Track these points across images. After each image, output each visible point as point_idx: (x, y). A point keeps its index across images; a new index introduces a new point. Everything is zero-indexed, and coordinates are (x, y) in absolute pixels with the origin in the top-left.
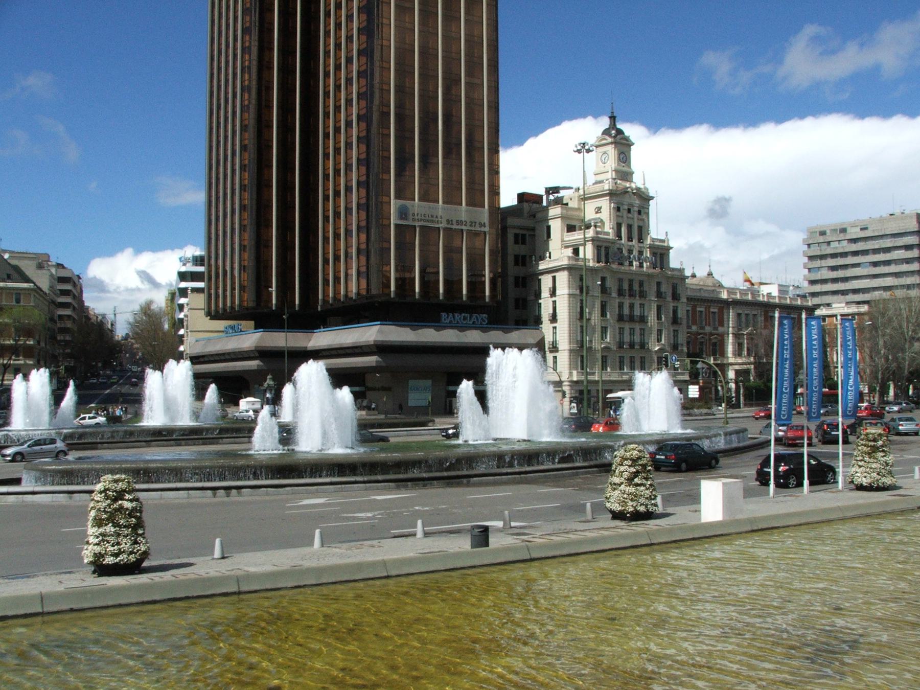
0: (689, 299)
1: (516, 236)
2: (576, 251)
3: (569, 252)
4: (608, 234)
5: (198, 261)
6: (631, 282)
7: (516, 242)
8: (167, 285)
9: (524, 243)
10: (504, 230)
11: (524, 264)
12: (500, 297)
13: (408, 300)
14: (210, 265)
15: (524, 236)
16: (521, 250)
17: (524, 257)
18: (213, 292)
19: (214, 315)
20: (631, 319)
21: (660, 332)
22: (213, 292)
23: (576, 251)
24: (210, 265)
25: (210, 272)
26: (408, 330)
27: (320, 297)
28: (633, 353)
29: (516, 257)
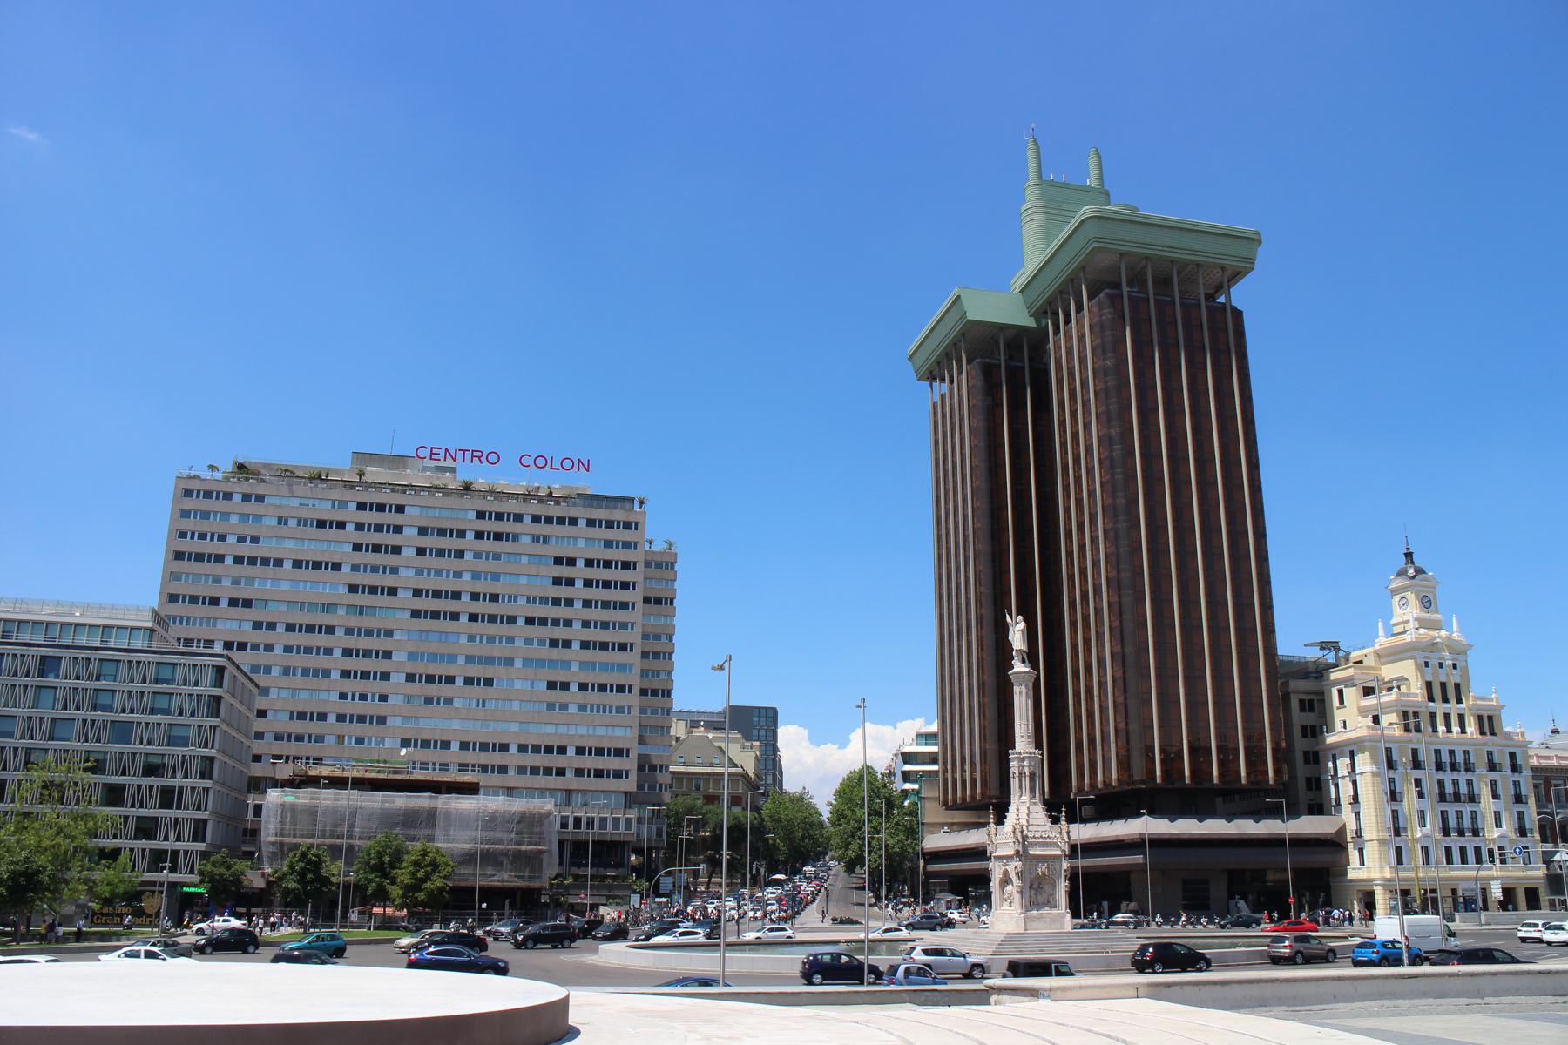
0: (1534, 769)
1: (1302, 702)
2: (1376, 720)
3: (1369, 721)
4: (1415, 695)
5: (927, 738)
6: (1452, 753)
7: (1302, 709)
8: (1384, 945)
9: (1311, 709)
10: (1286, 697)
11: (1314, 735)
12: (1286, 777)
13: (1178, 785)
14: (945, 764)
15: (1311, 702)
16: (1309, 718)
17: (1313, 727)
18: (949, 776)
19: (947, 807)
20: (1457, 797)
21: (1422, 814)
22: (949, 776)
23: (1376, 720)
24: (945, 764)
25: (945, 752)
26: (1223, 822)
27: (1074, 783)
28: (1462, 841)
29: (1304, 728)
